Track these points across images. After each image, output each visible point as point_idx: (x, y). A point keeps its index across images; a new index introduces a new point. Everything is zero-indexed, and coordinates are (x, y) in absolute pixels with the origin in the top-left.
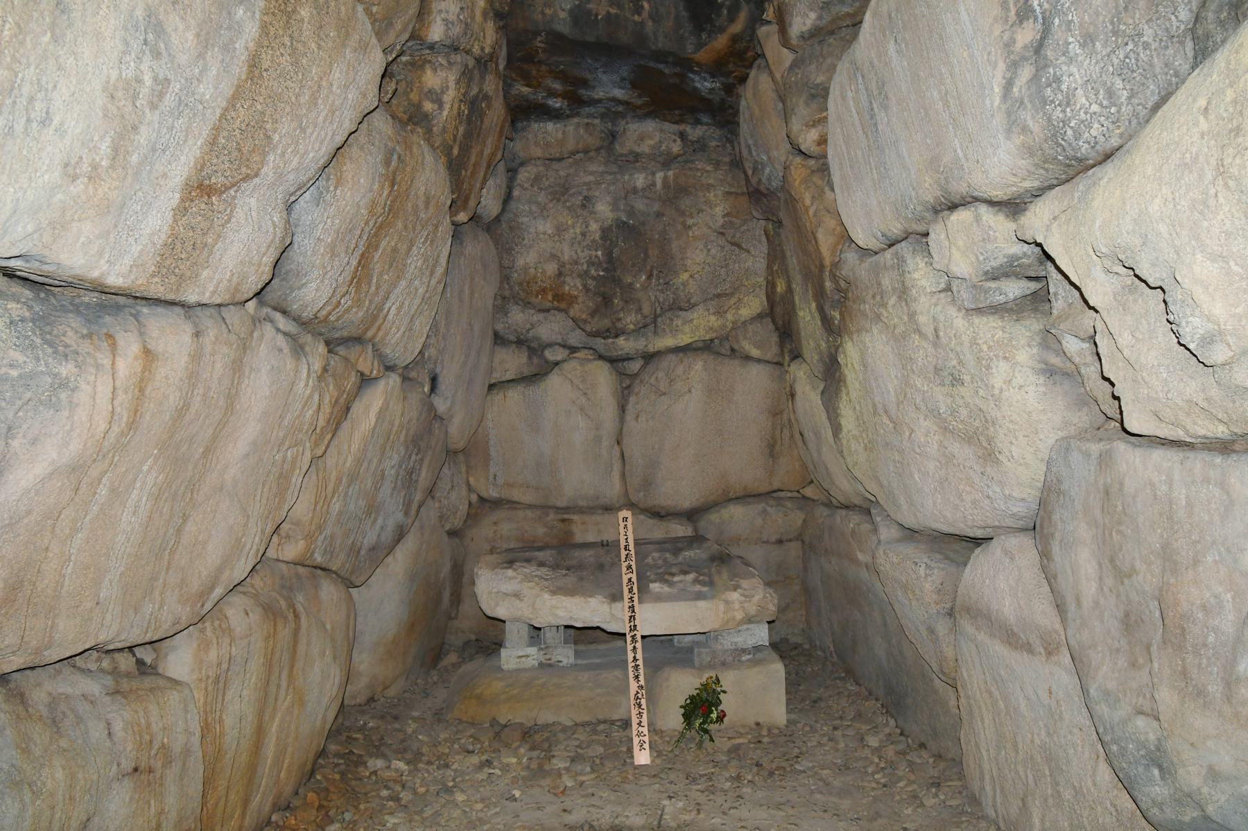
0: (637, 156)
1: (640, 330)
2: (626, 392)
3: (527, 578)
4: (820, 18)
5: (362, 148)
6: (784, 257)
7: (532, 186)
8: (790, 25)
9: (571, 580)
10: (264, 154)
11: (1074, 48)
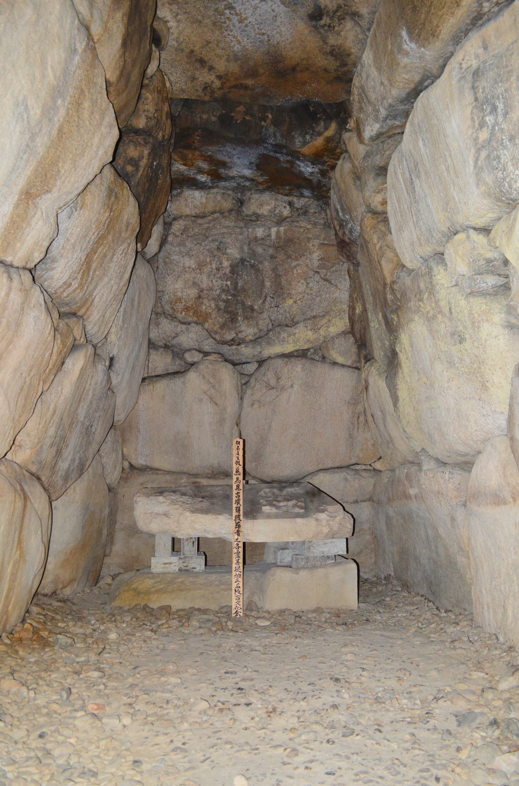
0: (258, 217)
1: (256, 341)
2: (244, 387)
3: (173, 502)
4: (382, 127)
5: (96, 187)
6: (361, 286)
7: (182, 234)
8: (364, 131)
9: (205, 504)
10: (56, 180)
11: (506, 142)
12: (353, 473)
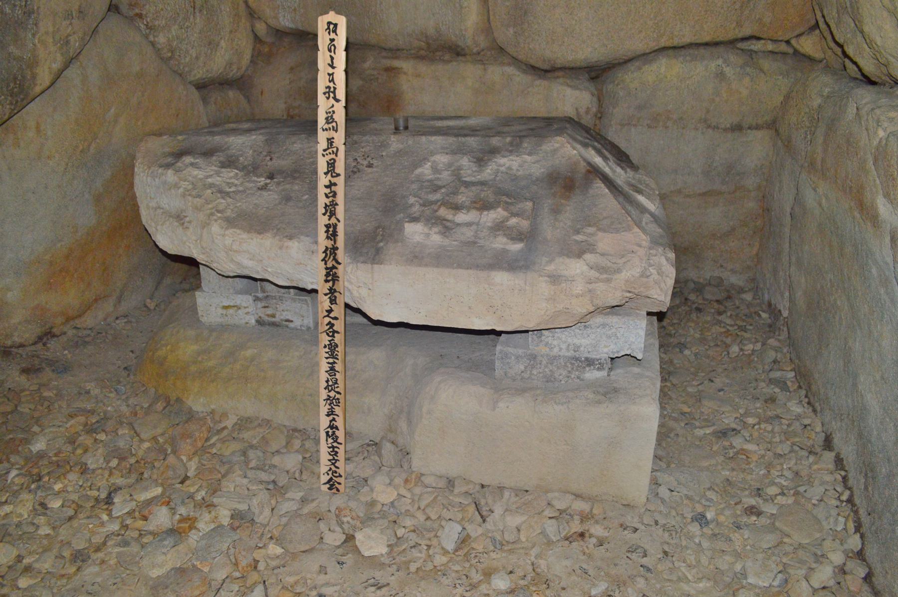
12: (741, 61)
